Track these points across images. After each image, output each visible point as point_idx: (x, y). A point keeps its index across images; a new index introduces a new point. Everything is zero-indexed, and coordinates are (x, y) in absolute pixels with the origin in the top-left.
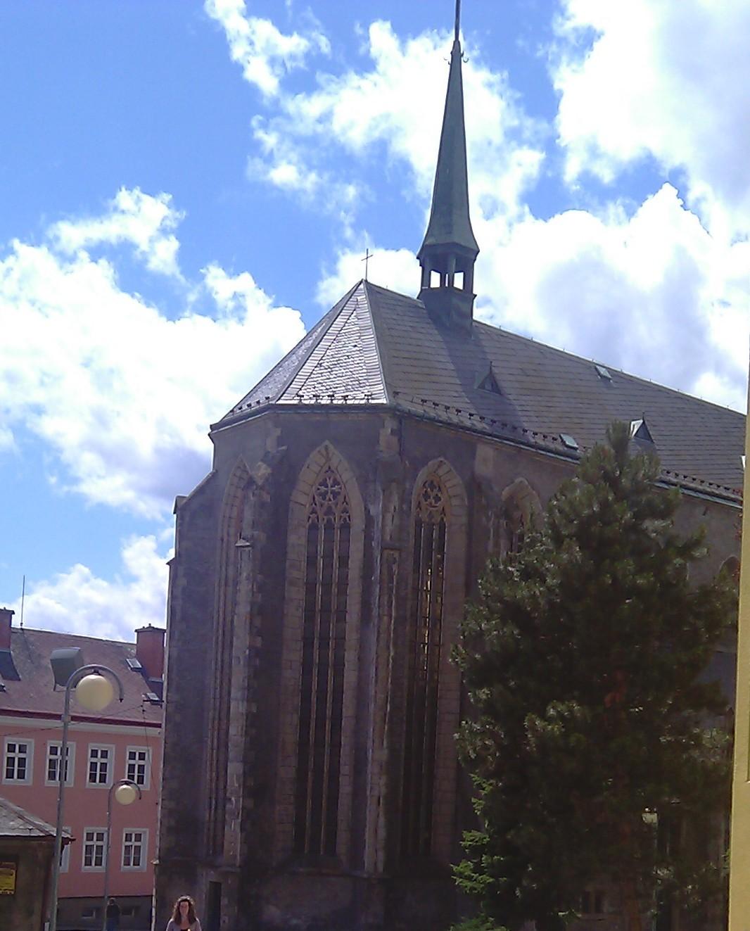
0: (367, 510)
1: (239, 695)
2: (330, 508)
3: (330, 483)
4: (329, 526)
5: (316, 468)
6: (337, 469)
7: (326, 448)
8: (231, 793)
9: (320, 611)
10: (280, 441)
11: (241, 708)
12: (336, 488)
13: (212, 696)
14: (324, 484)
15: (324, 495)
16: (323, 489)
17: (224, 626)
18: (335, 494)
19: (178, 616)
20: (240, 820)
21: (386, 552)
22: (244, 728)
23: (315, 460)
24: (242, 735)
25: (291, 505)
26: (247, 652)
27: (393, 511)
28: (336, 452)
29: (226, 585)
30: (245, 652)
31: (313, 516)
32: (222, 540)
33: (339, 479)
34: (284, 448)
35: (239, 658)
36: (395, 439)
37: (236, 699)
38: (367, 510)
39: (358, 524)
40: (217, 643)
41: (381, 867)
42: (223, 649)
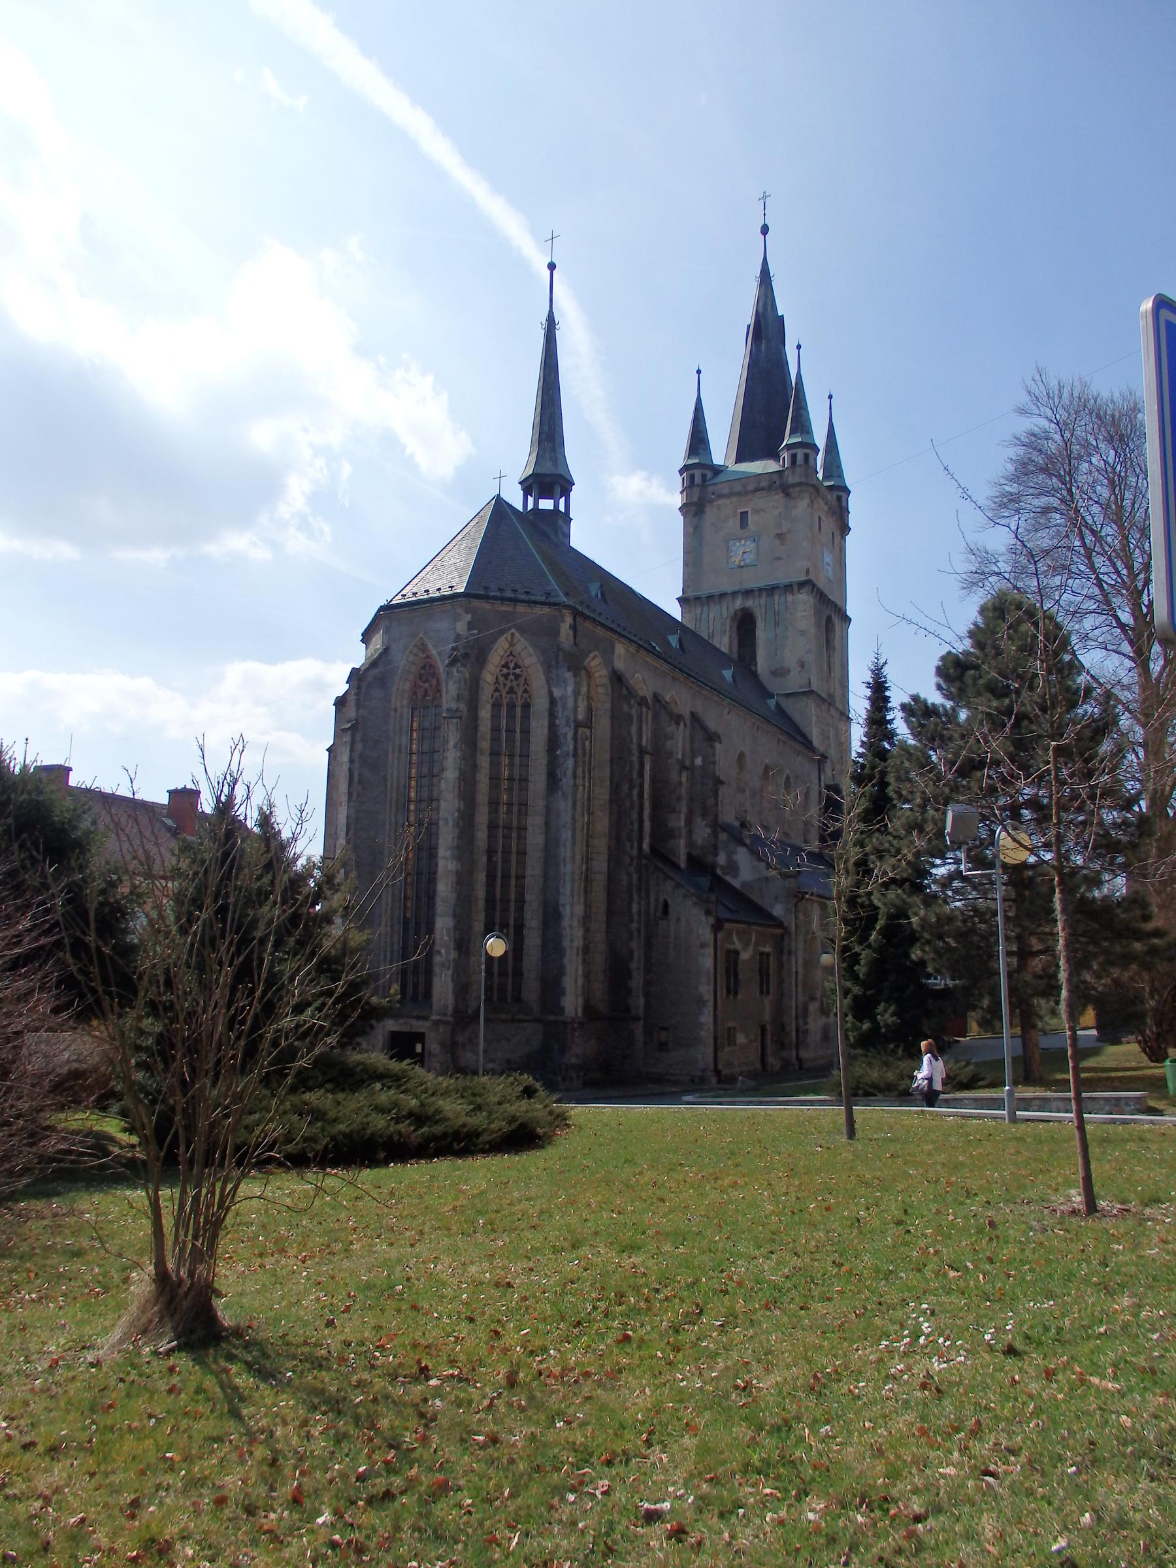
0: (551, 693)
1: (448, 853)
2: (511, 689)
3: (512, 665)
4: (512, 706)
5: (501, 652)
7: (513, 635)
10: (471, 626)
12: (518, 671)
14: (506, 666)
15: (506, 676)
16: (505, 671)
18: (517, 677)
19: (356, 778)
20: (450, 972)
21: (581, 730)
23: (502, 645)
28: (522, 640)
29: (400, 752)
31: (497, 694)
33: (520, 663)
36: (571, 633)
38: (551, 693)
39: (540, 704)
41: (580, 1013)
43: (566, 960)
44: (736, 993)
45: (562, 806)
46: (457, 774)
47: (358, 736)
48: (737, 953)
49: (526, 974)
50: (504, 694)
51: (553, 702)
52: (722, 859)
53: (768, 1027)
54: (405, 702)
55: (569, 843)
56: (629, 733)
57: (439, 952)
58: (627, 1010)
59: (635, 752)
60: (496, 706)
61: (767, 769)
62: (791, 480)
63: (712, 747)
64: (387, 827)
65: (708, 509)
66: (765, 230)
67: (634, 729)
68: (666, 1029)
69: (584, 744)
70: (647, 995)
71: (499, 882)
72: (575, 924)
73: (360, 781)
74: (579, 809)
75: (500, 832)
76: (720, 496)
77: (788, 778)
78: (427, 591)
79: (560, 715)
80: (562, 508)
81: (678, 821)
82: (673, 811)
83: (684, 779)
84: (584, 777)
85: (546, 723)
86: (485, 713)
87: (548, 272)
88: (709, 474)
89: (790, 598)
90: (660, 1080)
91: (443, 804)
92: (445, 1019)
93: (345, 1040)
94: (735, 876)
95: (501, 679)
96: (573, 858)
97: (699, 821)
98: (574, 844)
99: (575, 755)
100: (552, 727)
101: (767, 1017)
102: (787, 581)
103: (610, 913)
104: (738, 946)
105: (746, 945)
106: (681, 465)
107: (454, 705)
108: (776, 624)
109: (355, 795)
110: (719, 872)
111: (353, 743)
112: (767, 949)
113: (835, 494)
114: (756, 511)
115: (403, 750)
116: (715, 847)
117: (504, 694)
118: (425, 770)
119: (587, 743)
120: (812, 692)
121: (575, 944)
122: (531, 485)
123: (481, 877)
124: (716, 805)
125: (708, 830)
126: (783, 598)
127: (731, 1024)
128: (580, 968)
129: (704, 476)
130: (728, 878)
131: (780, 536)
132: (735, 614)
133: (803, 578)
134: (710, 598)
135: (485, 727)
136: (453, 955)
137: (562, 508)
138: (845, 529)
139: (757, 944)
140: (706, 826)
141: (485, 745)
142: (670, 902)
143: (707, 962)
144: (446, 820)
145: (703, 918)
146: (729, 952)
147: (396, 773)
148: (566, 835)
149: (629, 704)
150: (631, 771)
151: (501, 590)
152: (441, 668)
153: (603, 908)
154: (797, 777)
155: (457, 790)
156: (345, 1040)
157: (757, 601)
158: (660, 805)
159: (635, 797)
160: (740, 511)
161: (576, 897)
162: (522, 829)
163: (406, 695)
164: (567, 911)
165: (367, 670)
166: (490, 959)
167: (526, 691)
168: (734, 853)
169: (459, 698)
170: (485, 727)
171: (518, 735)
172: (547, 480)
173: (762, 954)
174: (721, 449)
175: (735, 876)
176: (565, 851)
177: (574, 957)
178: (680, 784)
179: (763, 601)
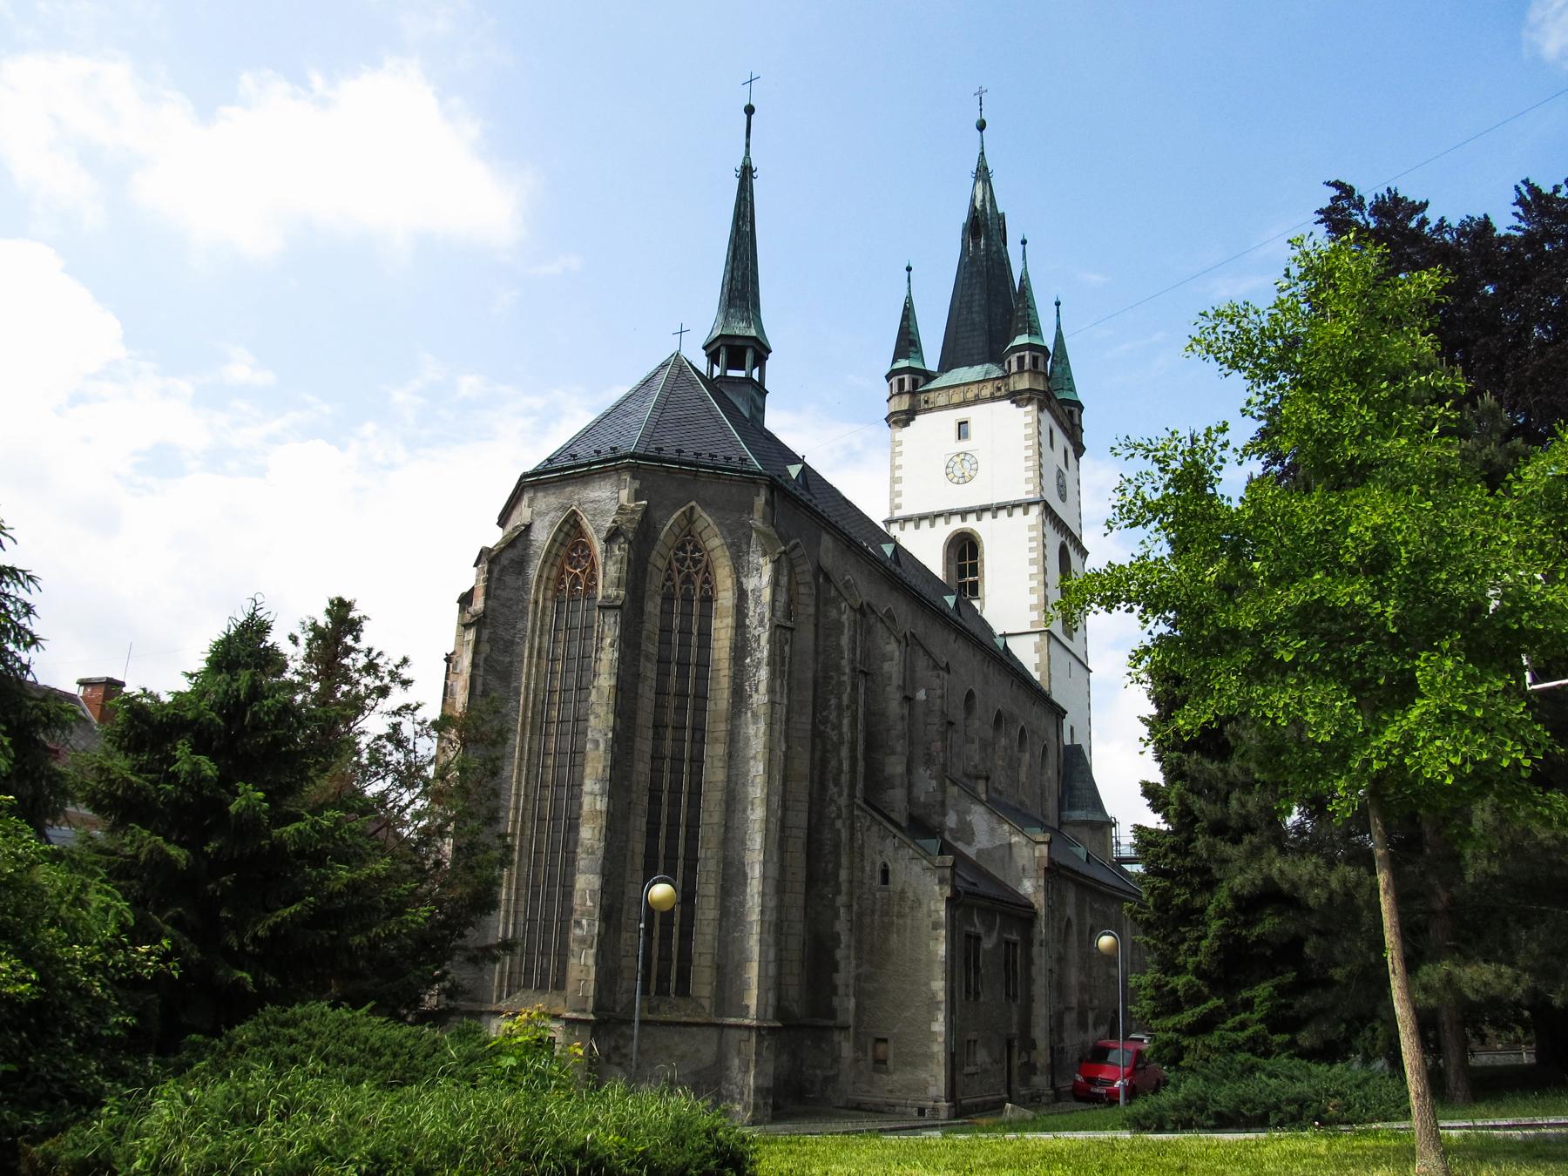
1: (597, 788)
2: (688, 576)
7: (692, 508)
9: (688, 696)
11: (598, 803)
13: (512, 804)
14: (682, 548)
15: (682, 561)
16: (681, 554)
18: (696, 562)
19: (479, 688)
20: (593, 951)
26: (610, 735)
31: (669, 583)
34: (644, 502)
37: (591, 793)
42: (532, 734)
44: (977, 995)
45: (751, 730)
46: (613, 682)
47: (486, 634)
48: (978, 938)
49: (696, 961)
52: (951, 820)
57: (578, 923)
58: (832, 1013)
61: (999, 715)
66: (981, 126)
68: (885, 1041)
70: (860, 994)
73: (485, 694)
75: (669, 733)
77: (1023, 730)
79: (751, 613)
81: (895, 766)
88: (921, 380)
90: (876, 1110)
91: (593, 721)
93: (349, 712)
94: (969, 843)
95: (675, 564)
97: (922, 772)
100: (740, 626)
101: (1014, 1030)
103: (811, 880)
104: (979, 929)
105: (990, 929)
106: (887, 370)
107: (612, 592)
110: (947, 836)
112: (1014, 937)
113: (1066, 408)
118: (572, 681)
119: (787, 648)
122: (718, 349)
123: (640, 823)
125: (934, 783)
130: (960, 846)
135: (652, 624)
138: (1079, 450)
140: (930, 777)
143: (941, 949)
144: (597, 743)
145: (937, 888)
146: (968, 936)
149: (839, 609)
152: (598, 547)
153: (801, 875)
154: (1033, 732)
155: (612, 702)
156: (349, 712)
158: (874, 744)
162: (698, 761)
165: (502, 551)
166: (650, 910)
167: (706, 581)
168: (968, 812)
171: (694, 640)
172: (739, 343)
173: (1007, 943)
174: (931, 352)
175: (969, 843)
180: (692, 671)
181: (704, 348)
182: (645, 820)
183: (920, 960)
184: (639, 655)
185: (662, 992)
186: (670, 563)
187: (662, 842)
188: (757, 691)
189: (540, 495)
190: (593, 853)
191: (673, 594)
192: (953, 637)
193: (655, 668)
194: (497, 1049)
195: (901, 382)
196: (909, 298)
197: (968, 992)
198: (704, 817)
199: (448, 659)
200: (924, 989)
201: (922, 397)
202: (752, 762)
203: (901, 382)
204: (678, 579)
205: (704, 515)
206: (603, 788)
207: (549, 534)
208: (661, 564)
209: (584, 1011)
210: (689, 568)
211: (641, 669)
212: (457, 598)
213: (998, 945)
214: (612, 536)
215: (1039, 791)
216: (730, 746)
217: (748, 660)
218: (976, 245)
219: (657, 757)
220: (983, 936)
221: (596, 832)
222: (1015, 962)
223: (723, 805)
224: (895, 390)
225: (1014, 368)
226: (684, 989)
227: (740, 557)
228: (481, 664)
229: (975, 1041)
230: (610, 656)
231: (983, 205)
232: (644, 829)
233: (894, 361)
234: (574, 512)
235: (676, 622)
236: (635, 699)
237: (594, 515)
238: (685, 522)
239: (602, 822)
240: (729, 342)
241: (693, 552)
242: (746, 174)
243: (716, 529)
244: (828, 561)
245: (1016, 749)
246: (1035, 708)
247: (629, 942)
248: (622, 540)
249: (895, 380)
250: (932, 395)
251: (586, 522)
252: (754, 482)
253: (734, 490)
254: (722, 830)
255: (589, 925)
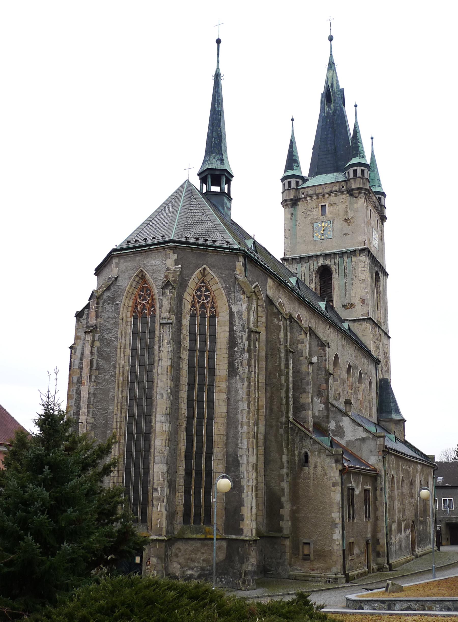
0: (230, 308)
1: (163, 419)
3: (203, 289)
4: (203, 317)
6: (209, 282)
7: (205, 269)
8: (158, 485)
9: (205, 368)
14: (199, 289)
15: (199, 297)
16: (199, 293)
17: (124, 374)
18: (207, 297)
20: (165, 504)
22: (167, 441)
24: (165, 446)
25: (184, 300)
26: (169, 391)
27: (253, 310)
29: (125, 348)
30: (167, 391)
31: (193, 309)
32: (123, 319)
34: (180, 266)
35: (162, 394)
36: (243, 269)
38: (230, 308)
40: (118, 384)
41: (254, 534)
43: (244, 496)
44: (353, 518)
45: (239, 386)
48: (353, 489)
50: (198, 309)
51: (232, 314)
52: (332, 426)
53: (370, 542)
54: (129, 314)
55: (245, 412)
56: (279, 338)
58: (280, 530)
59: (283, 351)
60: (193, 316)
61: (350, 365)
62: (353, 186)
63: (324, 350)
64: (116, 400)
65: (300, 203)
67: (282, 335)
68: (308, 544)
69: (255, 344)
71: (195, 438)
72: (250, 469)
73: (98, 368)
74: (252, 388)
76: (307, 196)
78: (145, 239)
79: (237, 324)
80: (226, 191)
82: (305, 392)
83: (310, 370)
84: (255, 367)
85: (227, 329)
86: (186, 321)
87: (217, 44)
88: (300, 182)
89: (354, 259)
92: (161, 538)
94: (342, 437)
95: (197, 298)
96: (249, 422)
98: (249, 413)
99: (249, 351)
100: (231, 331)
101: (369, 535)
102: (352, 249)
104: (354, 485)
105: (358, 484)
106: (282, 176)
107: (167, 315)
108: (346, 275)
109: (93, 377)
111: (93, 341)
112: (368, 487)
113: (377, 196)
114: (331, 205)
115: (127, 347)
116: (328, 417)
117: (198, 309)
120: (370, 319)
121: (251, 484)
124: (327, 389)
125: (322, 406)
126: (349, 259)
127: (351, 540)
128: (254, 500)
129: (297, 183)
131: (347, 220)
132: (319, 268)
133: (363, 247)
134: (302, 259)
135: (186, 331)
136: (166, 491)
137: (226, 191)
138: (383, 218)
139: (363, 484)
141: (186, 343)
142: (309, 454)
143: (338, 497)
145: (334, 465)
146: (349, 489)
147: (122, 363)
148: (243, 405)
150: (280, 363)
151: (197, 239)
152: (156, 290)
157: (333, 260)
159: (283, 382)
160: (320, 205)
161: (251, 450)
162: (211, 402)
163: (130, 309)
164: (244, 460)
167: (213, 307)
168: (341, 421)
169: (170, 311)
170: (186, 331)
171: (207, 338)
172: (217, 173)
173: (365, 490)
175: (342, 437)
176: (243, 417)
177: (250, 493)
178: (309, 373)
179: (336, 261)
180: (207, 354)
181: (198, 175)
182: (185, 433)
183: (325, 502)
184: (180, 347)
185: (197, 522)
186: (193, 298)
187: (194, 444)
188: (241, 365)
189: (122, 261)
190: (162, 453)
191: (195, 314)
192: (328, 327)
193: (188, 353)
194: (405, 596)
195: (290, 183)
196: (293, 136)
197: (349, 517)
198: (216, 431)
199: (71, 348)
200: (328, 517)
201: (301, 190)
202: (240, 403)
203: (290, 183)
204: (198, 306)
205: (210, 272)
206: (166, 419)
207: (128, 282)
208: (189, 298)
209: (160, 535)
210: (203, 300)
211: (181, 355)
212: (74, 315)
213: (361, 492)
214: (167, 285)
215: (368, 404)
216: (227, 395)
217: (236, 349)
218: (329, 107)
219: (190, 401)
220: (355, 488)
221: (164, 442)
222: (369, 500)
223: (225, 425)
224: (287, 187)
225: (351, 176)
226: (208, 520)
227: (230, 294)
228: (96, 352)
229: (353, 542)
230: (167, 350)
231: (332, 84)
232: (185, 438)
233: (286, 171)
234: (142, 271)
235: (198, 329)
236: (179, 370)
237: (153, 273)
238: (201, 276)
239: (166, 436)
240: (212, 172)
241: (205, 292)
242: (217, 77)
243: (217, 279)
244: (270, 293)
245: (357, 383)
246: (366, 361)
247: (180, 498)
248: (171, 287)
249: (286, 182)
250: (306, 190)
251: (148, 276)
252: (236, 254)
253: (226, 258)
254: (225, 438)
255: (161, 490)
